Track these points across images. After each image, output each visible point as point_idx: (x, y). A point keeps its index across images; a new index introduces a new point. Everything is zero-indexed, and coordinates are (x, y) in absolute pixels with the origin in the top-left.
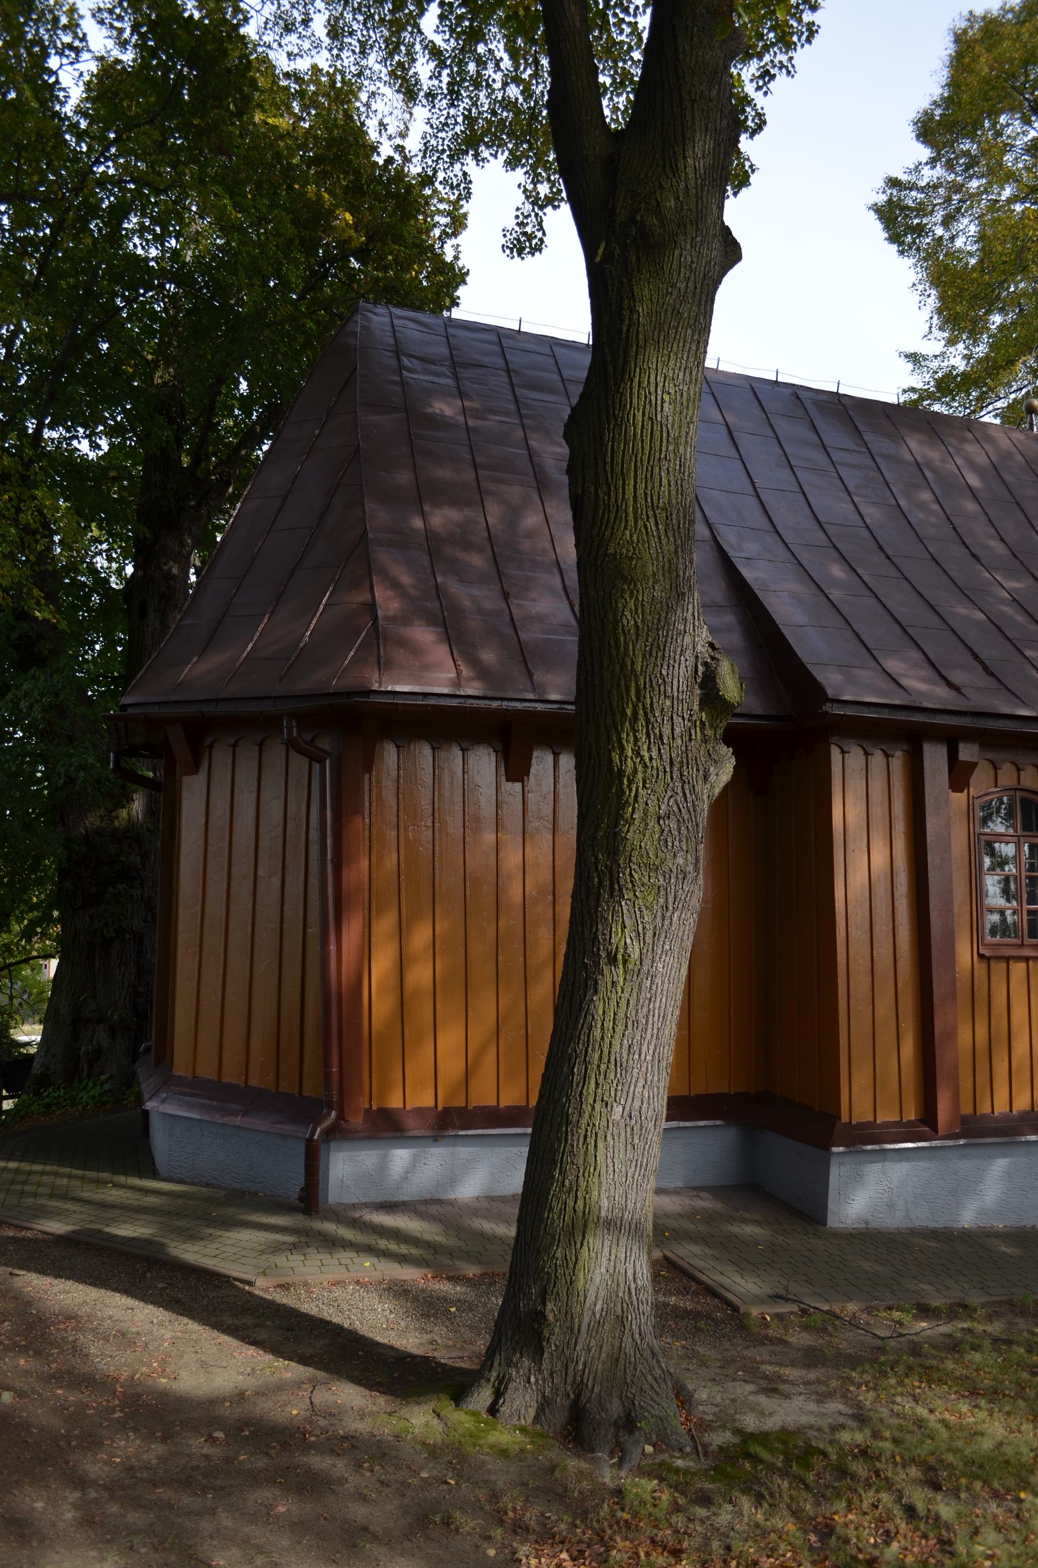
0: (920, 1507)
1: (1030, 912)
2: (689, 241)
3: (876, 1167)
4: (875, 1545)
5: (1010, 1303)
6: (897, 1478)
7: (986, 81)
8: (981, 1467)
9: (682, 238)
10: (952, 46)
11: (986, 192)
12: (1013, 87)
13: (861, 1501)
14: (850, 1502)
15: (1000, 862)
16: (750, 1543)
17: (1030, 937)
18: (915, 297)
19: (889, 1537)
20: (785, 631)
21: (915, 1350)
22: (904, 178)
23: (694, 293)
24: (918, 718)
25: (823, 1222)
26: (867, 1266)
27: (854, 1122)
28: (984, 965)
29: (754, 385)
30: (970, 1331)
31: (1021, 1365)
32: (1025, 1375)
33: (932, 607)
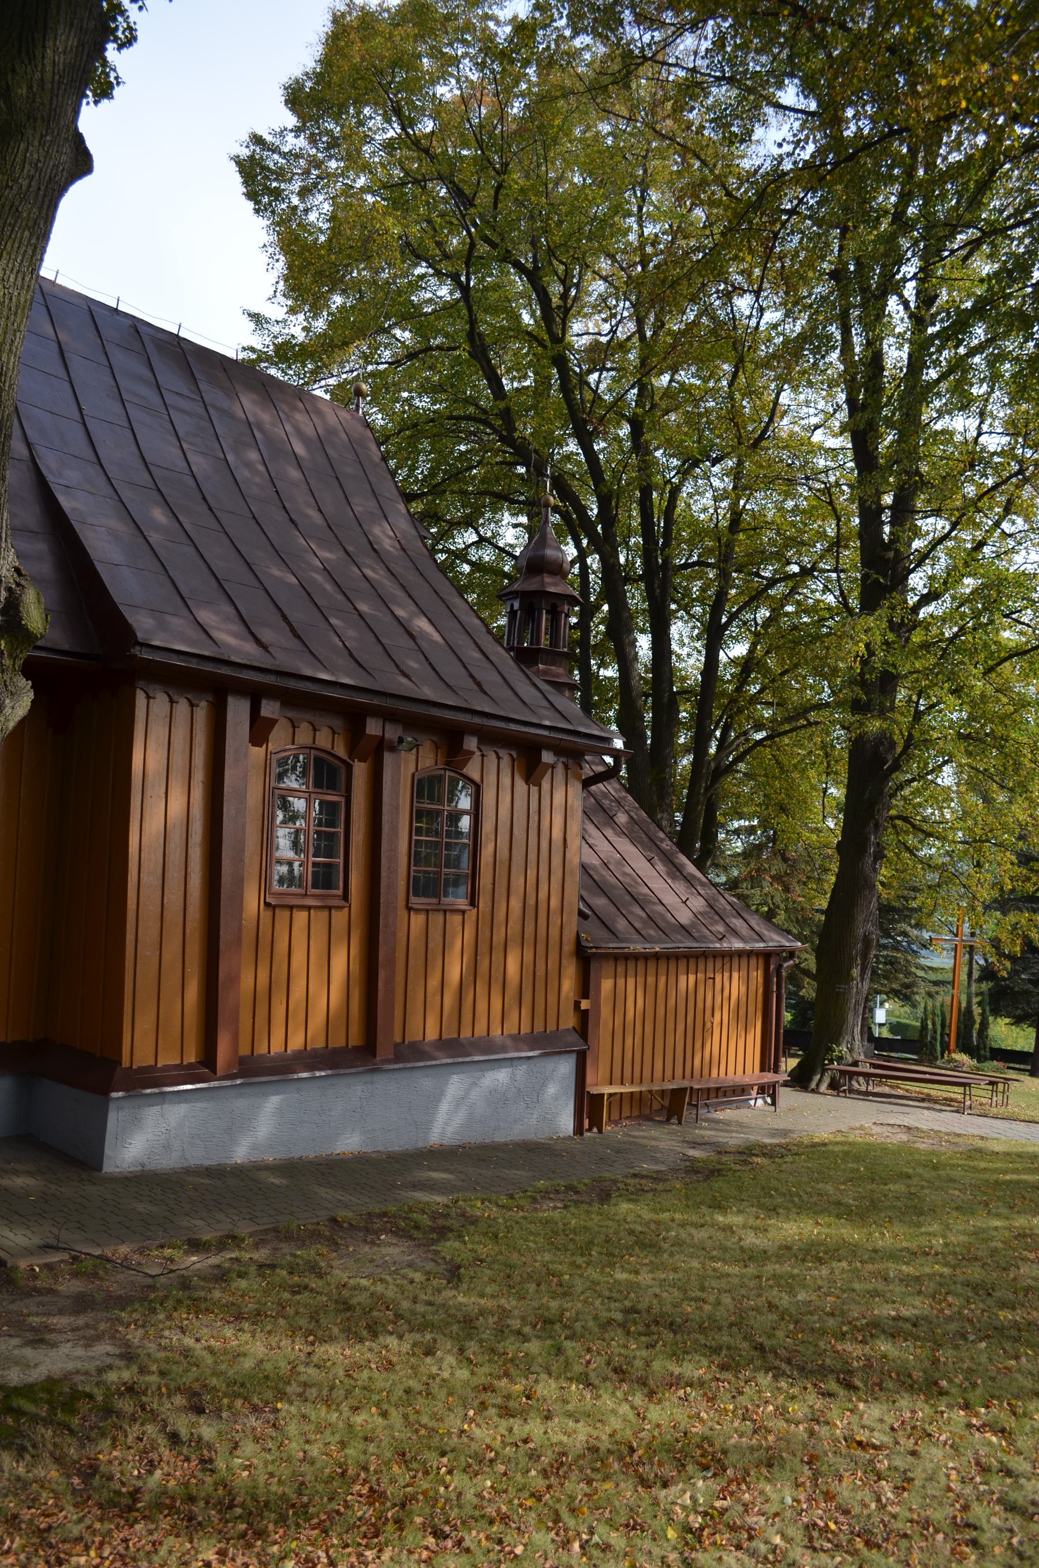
0: (184, 1433)
1: (315, 864)
2: (38, 136)
3: (155, 1110)
4: (139, 1477)
5: (276, 1230)
6: (162, 1409)
7: (356, 69)
8: (242, 1385)
9: (30, 131)
10: (329, 24)
11: (342, 175)
12: (379, 83)
13: (126, 1436)
14: (114, 1439)
15: (292, 817)
16: (11, 1498)
17: (314, 886)
18: (264, 258)
19: (152, 1466)
20: (100, 568)
21: (185, 1284)
22: (269, 138)
23: (37, 194)
24: (225, 671)
25: (99, 1168)
26: (141, 1207)
27: (135, 1067)
28: (270, 913)
29: (93, 307)
30: (237, 1260)
31: (283, 1286)
32: (286, 1295)
33: (248, 564)
